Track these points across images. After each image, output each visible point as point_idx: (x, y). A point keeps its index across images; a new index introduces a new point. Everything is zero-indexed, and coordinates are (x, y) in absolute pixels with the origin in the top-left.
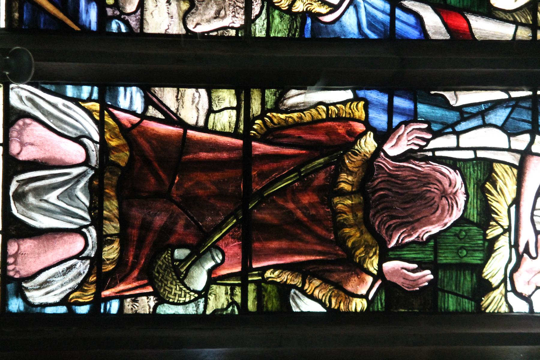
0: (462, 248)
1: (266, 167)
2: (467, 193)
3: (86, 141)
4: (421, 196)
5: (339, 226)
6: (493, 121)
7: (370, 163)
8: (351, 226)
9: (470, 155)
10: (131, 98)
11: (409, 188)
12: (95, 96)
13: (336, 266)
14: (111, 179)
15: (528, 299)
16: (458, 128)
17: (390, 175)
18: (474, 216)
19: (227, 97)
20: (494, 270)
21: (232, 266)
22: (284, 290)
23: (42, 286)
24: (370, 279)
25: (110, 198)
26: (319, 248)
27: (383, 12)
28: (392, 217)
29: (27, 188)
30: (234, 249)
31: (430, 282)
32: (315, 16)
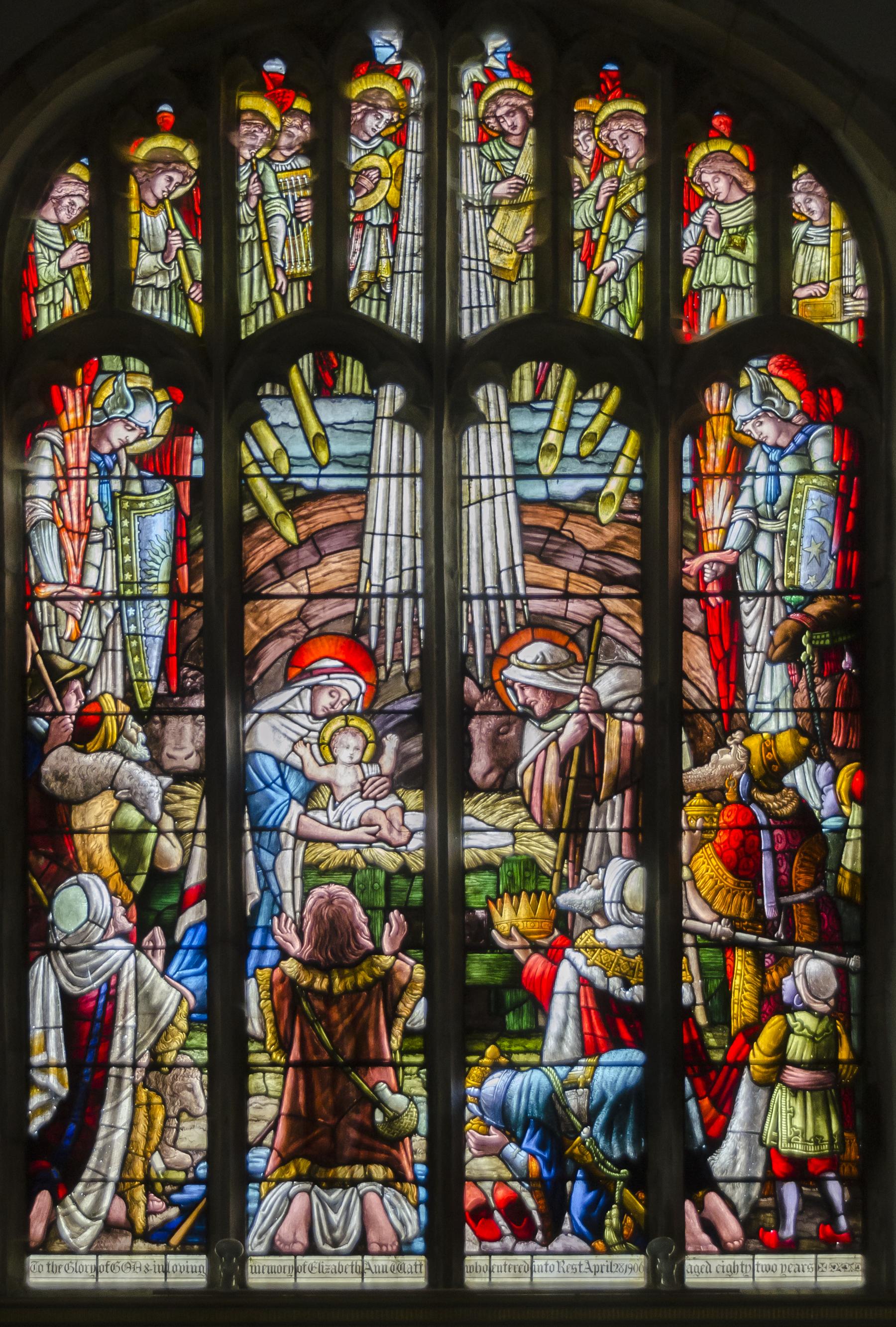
0: (372, 887)
1: (310, 1049)
2: (328, 884)
3: (291, 1192)
4: (332, 921)
5: (356, 989)
6: (271, 863)
7: (307, 965)
8: (356, 979)
9: (298, 882)
10: (258, 1160)
11: (325, 931)
12: (256, 1185)
13: (388, 990)
14: (321, 1173)
15: (412, 833)
16: (277, 892)
17: (315, 947)
18: (348, 877)
19: (255, 1081)
20: (388, 859)
21: (388, 1075)
22: (407, 1033)
23: (403, 1224)
24: (398, 962)
25: (336, 1173)
26: (374, 1004)
27: (185, 955)
28: (349, 945)
29: (329, 1237)
30: (375, 1074)
31: (401, 912)
32: (190, 1012)
